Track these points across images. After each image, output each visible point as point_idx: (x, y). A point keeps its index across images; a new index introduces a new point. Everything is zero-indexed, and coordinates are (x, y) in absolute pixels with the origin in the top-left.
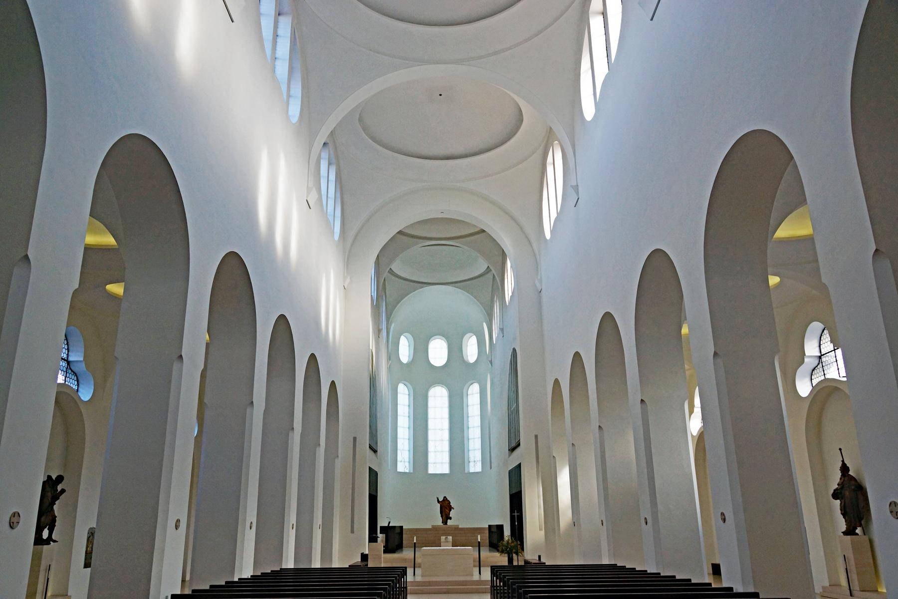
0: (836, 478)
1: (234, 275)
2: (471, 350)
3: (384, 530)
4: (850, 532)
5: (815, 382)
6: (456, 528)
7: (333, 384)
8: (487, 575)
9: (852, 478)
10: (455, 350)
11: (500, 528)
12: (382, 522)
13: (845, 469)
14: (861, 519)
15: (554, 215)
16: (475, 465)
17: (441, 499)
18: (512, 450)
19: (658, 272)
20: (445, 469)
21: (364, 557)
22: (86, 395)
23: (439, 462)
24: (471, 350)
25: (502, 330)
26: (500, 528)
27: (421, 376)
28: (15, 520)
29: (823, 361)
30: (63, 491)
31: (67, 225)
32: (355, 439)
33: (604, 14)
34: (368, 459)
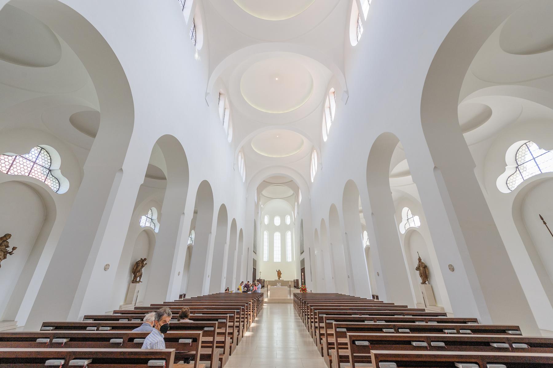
0: (416, 264)
1: (205, 190)
2: (288, 221)
3: (258, 281)
4: (424, 283)
6: (283, 281)
7: (241, 230)
8: (292, 297)
9: (422, 263)
11: (297, 280)
12: (257, 278)
13: (420, 260)
14: (427, 278)
16: (289, 259)
18: (302, 253)
19: (350, 188)
20: (280, 261)
22: (157, 230)
23: (277, 258)
24: (288, 221)
25: (298, 213)
26: (297, 280)
27: (272, 229)
28: (107, 267)
29: (410, 221)
30: (146, 264)
33: (330, 108)
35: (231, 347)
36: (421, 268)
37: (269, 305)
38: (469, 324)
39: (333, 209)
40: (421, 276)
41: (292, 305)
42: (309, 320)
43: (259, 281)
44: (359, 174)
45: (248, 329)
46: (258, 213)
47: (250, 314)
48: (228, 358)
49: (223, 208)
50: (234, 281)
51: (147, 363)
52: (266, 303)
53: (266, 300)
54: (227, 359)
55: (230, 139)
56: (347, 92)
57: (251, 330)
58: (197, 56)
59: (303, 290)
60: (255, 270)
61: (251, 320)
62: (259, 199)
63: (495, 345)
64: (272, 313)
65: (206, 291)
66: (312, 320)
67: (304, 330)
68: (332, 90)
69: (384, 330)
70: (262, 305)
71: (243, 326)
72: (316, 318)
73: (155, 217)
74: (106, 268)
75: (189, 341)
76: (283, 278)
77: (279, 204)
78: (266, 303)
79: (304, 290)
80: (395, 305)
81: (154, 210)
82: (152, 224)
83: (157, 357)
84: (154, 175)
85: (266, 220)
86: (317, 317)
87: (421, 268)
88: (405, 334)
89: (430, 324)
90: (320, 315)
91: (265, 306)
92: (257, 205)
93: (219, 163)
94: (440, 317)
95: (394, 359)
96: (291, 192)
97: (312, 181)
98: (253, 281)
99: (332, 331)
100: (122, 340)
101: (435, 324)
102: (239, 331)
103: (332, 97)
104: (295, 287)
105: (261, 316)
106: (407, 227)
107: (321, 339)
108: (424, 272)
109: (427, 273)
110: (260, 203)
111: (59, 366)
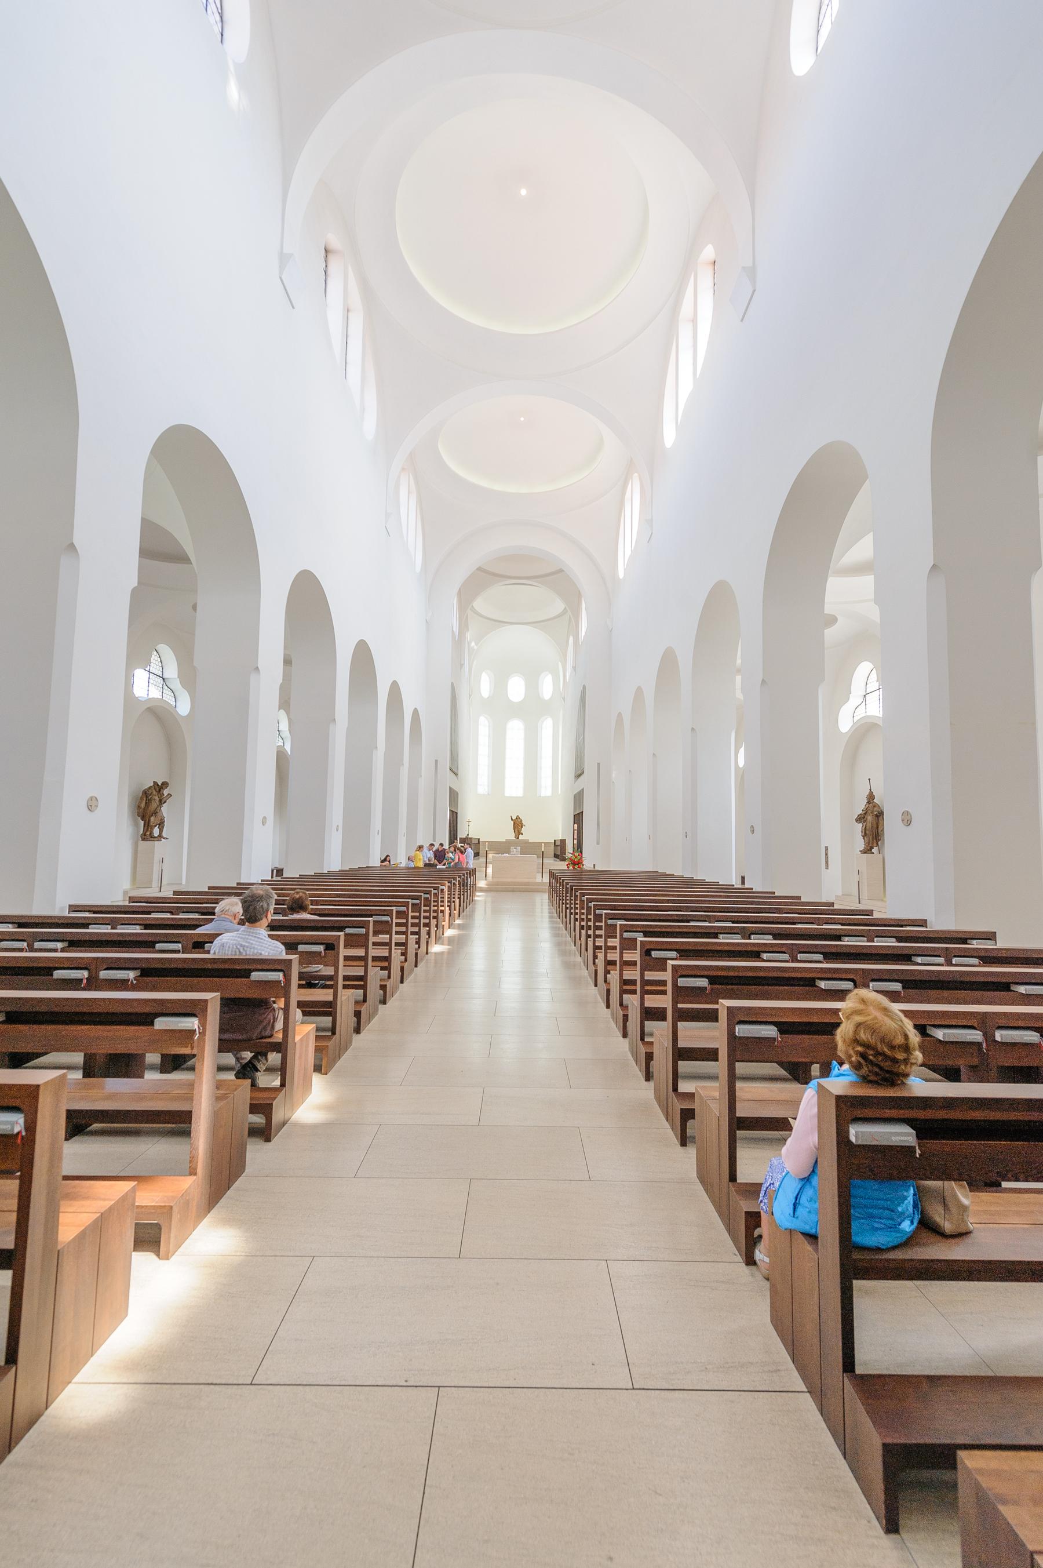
1: (308, 599)
3: (463, 841)
4: (868, 850)
5: (856, 719)
6: (526, 842)
7: (416, 712)
8: (546, 879)
10: (532, 686)
11: (563, 842)
13: (871, 797)
14: (878, 840)
15: (628, 553)
16: (546, 788)
17: (437, 846)
19: (718, 602)
20: (520, 793)
21: (832, 620)
22: (184, 708)
23: (514, 786)
24: (547, 687)
25: (574, 668)
26: (563, 842)
28: (93, 803)
29: (862, 698)
30: (170, 795)
31: (110, 507)
32: (436, 761)
33: (694, 321)
34: (449, 780)
35: (402, 969)
36: (869, 818)
37: (490, 894)
38: (975, 944)
39: (668, 662)
40: (864, 835)
41: (546, 896)
42: (583, 932)
43: (465, 840)
44: (744, 563)
45: (438, 940)
46: (462, 665)
47: (442, 911)
48: (397, 988)
49: (363, 655)
50: (402, 842)
51: (248, 976)
52: (481, 890)
53: (481, 884)
54: (395, 989)
55: (370, 425)
56: (751, 272)
57: (446, 942)
58: (233, 91)
59: (574, 863)
60: (454, 815)
61: (446, 924)
62: (464, 625)
63: (1022, 989)
64: (496, 911)
65: (334, 862)
66: (583, 923)
67: (566, 943)
68: (709, 252)
69: (765, 956)
70: (473, 894)
71: (429, 933)
72: (600, 928)
73: (172, 672)
74: (92, 805)
75: (320, 948)
76: (527, 835)
77: (523, 640)
78: (481, 890)
79: (577, 863)
80: (876, 915)
81: (165, 650)
82: (167, 691)
83: (267, 967)
84: (158, 550)
85: (486, 687)
86: (603, 924)
87: (869, 818)
88: (812, 963)
89: (878, 942)
90: (610, 922)
91: (479, 897)
92: (459, 642)
93: (341, 518)
94: (908, 928)
95: (706, 973)
96: (559, 606)
97: (621, 575)
98: (451, 842)
99: (614, 942)
100: (180, 945)
101: (892, 943)
102: (418, 942)
103: (705, 280)
104: (556, 856)
105: (471, 916)
106: (860, 713)
107: (595, 957)
108: (872, 826)
109: (880, 828)
110: (469, 635)
111: (81, 980)
